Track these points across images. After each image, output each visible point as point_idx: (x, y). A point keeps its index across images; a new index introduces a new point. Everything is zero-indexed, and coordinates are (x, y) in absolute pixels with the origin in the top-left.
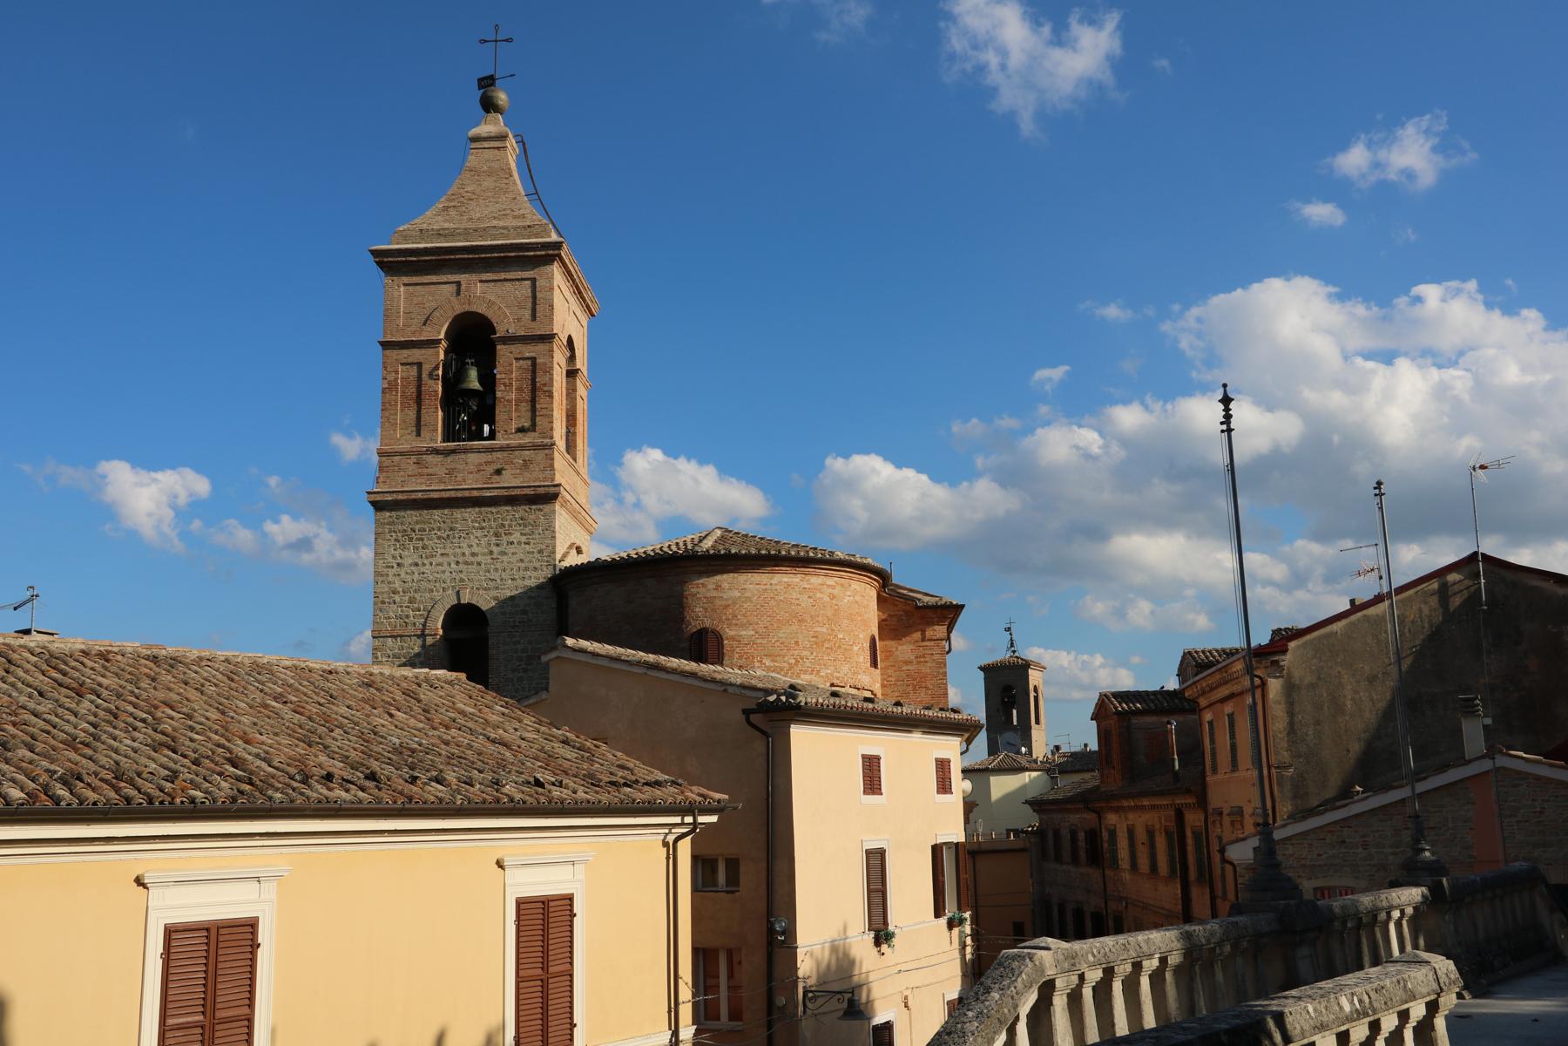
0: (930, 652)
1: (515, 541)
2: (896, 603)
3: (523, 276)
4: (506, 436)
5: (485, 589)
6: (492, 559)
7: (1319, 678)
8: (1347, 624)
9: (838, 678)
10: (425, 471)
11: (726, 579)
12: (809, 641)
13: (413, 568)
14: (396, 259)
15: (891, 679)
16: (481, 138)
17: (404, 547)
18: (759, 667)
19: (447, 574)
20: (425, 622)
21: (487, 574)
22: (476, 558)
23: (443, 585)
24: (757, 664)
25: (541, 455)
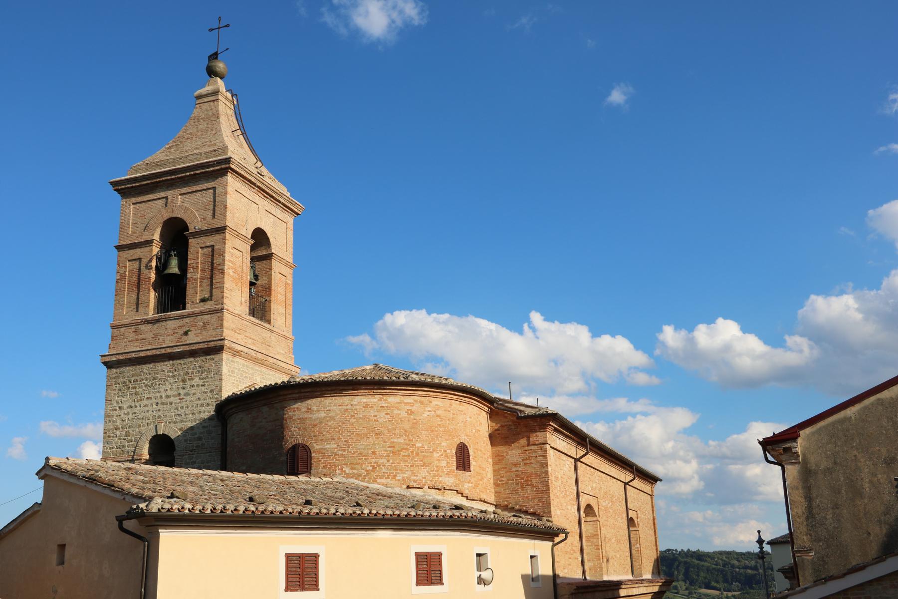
0: (534, 455)
1: (195, 384)
2: (506, 415)
3: (208, 187)
4: (193, 306)
5: (175, 423)
6: (180, 399)
7: (835, 463)
8: (861, 409)
9: (415, 481)
10: (140, 337)
11: (314, 403)
12: (386, 451)
13: (129, 410)
14: (126, 186)
15: (503, 479)
16: (203, 96)
17: (124, 395)
18: (339, 474)
19: (151, 413)
20: (135, 450)
21: (176, 411)
22: (169, 399)
23: (148, 421)
24: (338, 472)
25: (215, 316)
